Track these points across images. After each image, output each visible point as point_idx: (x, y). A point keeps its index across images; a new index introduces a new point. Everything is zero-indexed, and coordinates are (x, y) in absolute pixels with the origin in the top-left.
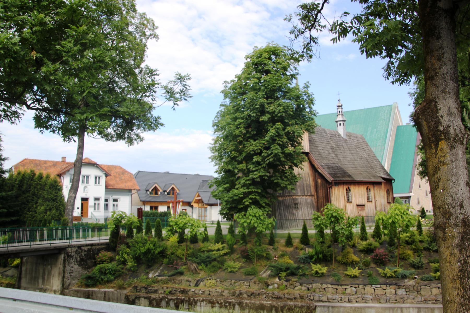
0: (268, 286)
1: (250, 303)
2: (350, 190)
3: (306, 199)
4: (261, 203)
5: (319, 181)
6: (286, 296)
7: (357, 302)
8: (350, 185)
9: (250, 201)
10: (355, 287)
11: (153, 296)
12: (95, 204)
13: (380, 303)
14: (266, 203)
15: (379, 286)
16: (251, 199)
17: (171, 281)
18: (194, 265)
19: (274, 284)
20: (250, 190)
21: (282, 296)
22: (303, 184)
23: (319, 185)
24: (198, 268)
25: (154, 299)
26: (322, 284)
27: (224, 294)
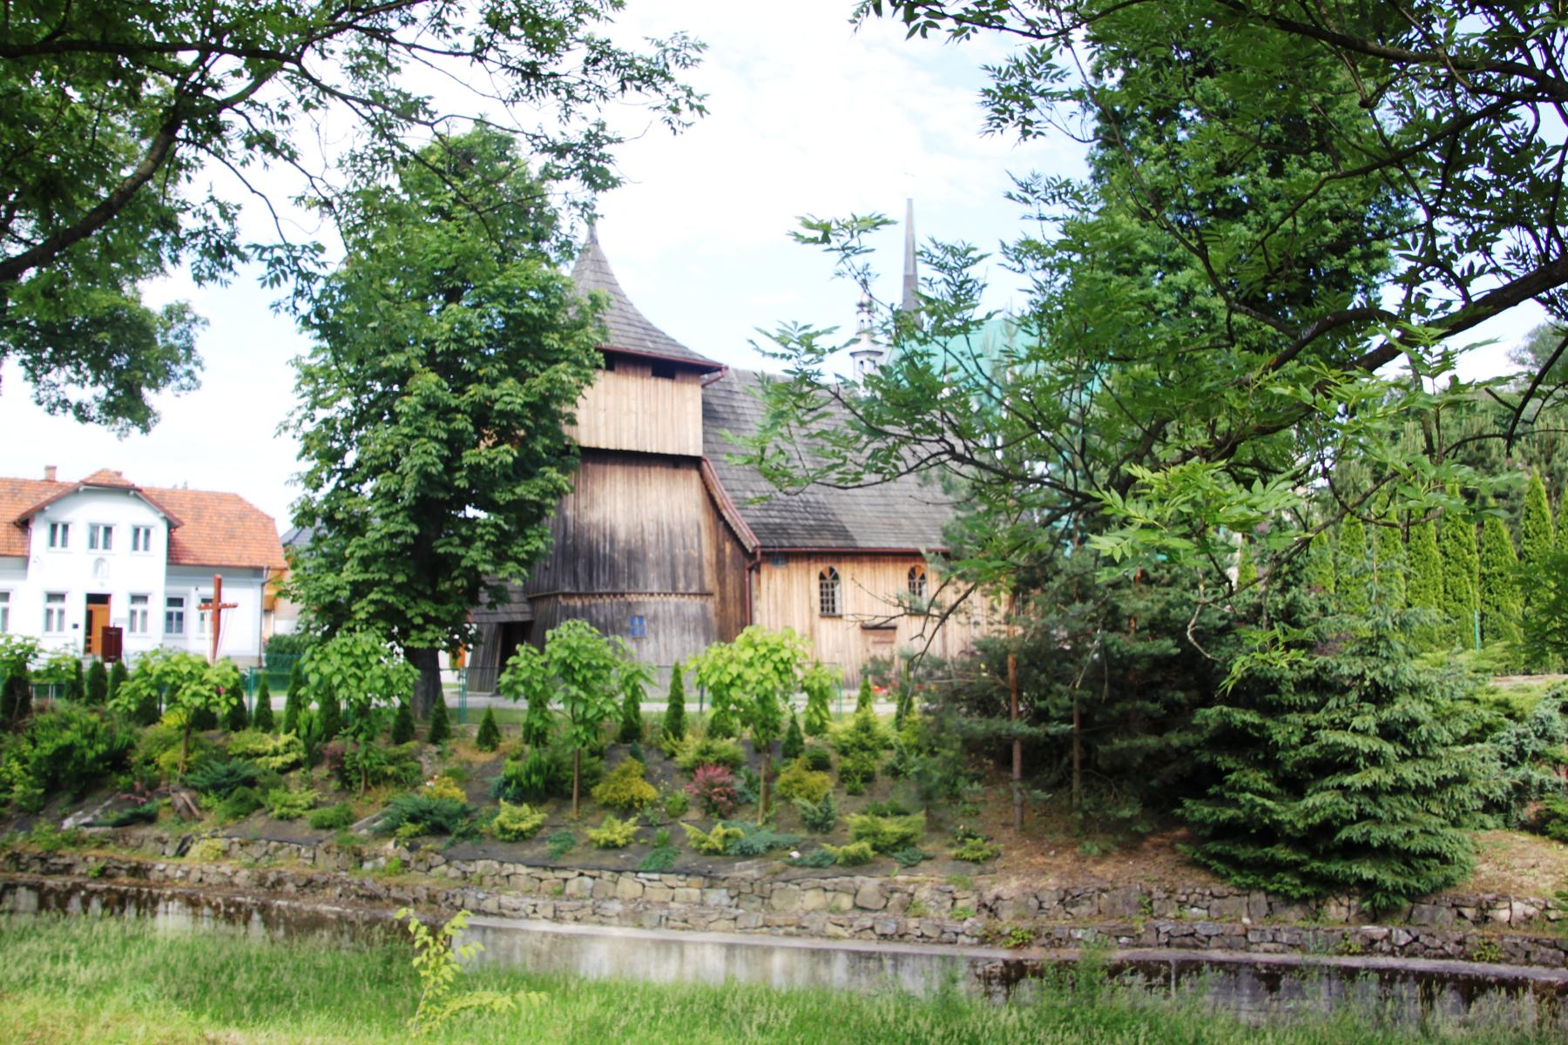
0: (361, 863)
1: (289, 907)
2: (836, 577)
3: (678, 607)
4: (410, 614)
5: (728, 547)
6: (394, 893)
7: (576, 919)
8: (839, 561)
9: (372, 609)
10: (593, 878)
11: (50, 882)
12: (133, 613)
13: (641, 926)
14: (425, 616)
15: (656, 876)
16: (372, 602)
17: (115, 839)
18: (183, 794)
19: (376, 856)
20: (368, 576)
21: (381, 891)
22: (673, 558)
23: (728, 560)
24: (196, 804)
25: (52, 890)
26: (502, 863)
27: (236, 880)
